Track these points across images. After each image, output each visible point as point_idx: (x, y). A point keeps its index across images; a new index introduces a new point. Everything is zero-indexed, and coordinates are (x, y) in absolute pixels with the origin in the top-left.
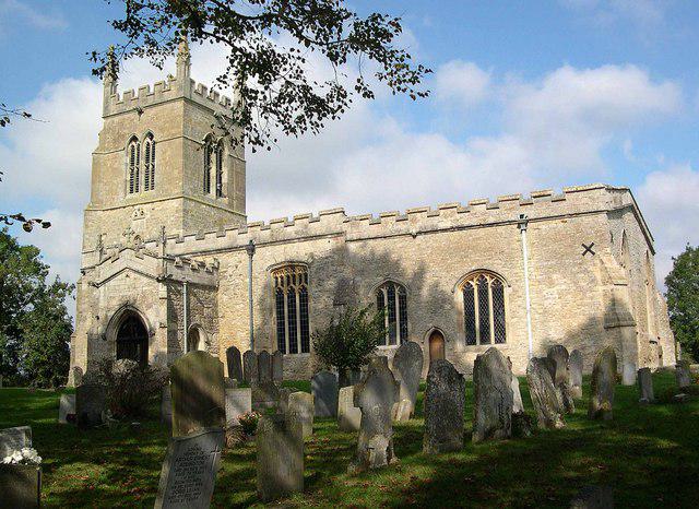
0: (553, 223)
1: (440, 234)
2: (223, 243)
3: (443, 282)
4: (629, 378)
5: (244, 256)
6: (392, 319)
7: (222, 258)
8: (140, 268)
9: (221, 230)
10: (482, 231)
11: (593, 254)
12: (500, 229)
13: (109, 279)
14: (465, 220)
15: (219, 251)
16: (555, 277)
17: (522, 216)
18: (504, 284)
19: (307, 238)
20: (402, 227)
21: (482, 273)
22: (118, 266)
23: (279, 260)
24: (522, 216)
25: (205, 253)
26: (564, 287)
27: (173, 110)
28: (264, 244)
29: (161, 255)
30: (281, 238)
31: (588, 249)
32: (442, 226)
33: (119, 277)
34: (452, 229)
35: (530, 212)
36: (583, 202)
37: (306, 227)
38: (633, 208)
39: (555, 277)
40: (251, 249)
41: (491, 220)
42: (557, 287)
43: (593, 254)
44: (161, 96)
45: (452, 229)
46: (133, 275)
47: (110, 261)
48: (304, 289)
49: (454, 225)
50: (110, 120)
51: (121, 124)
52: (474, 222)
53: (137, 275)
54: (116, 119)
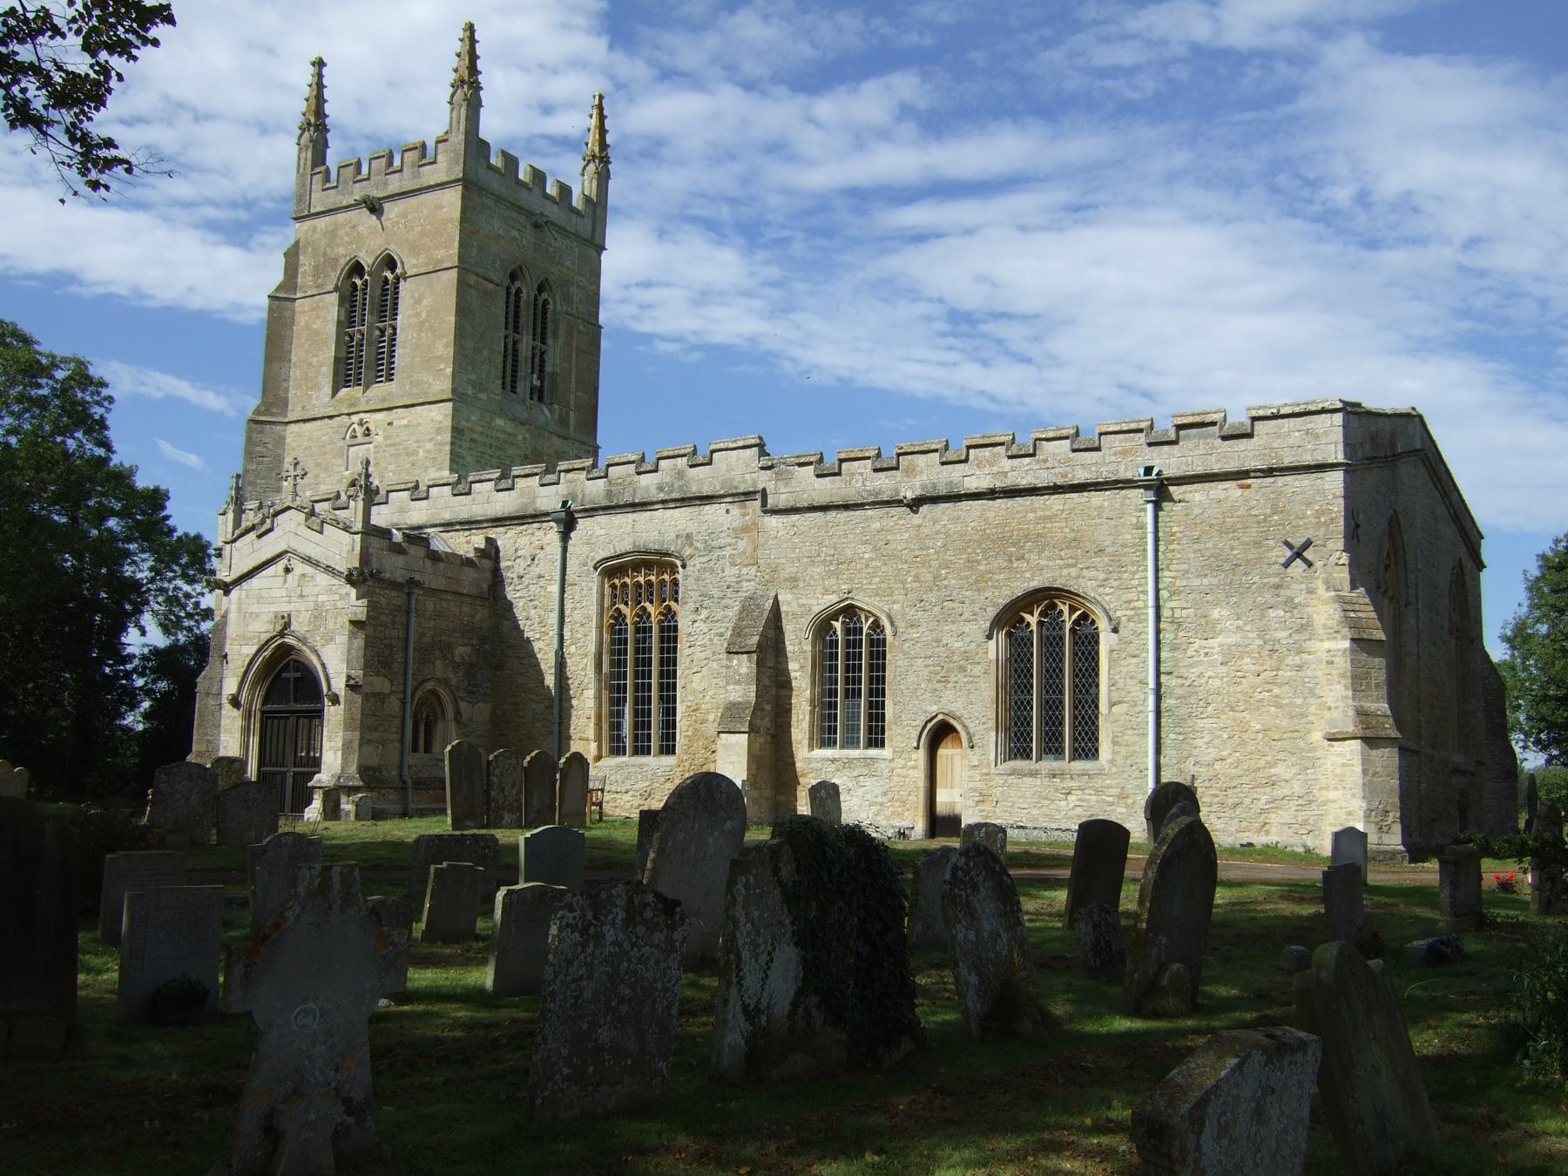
0: (1219, 489)
1: (965, 505)
2: (505, 503)
3: (1301, 570)
4: (1402, 848)
5: (550, 535)
6: (851, 694)
7: (506, 539)
8: (315, 553)
9: (503, 477)
10: (1056, 501)
11: (1310, 564)
12: (1096, 498)
13: (249, 575)
14: (1023, 473)
15: (498, 521)
16: (1215, 613)
17: (1148, 470)
18: (1103, 625)
19: (686, 501)
20: (885, 484)
21: (1046, 597)
22: (270, 546)
23: (621, 549)
24: (1148, 470)
25: (469, 524)
26: (1232, 640)
27: (440, 207)
28: (591, 512)
29: (358, 526)
30: (627, 498)
31: (1299, 555)
32: (972, 484)
33: (271, 570)
34: (991, 494)
35: (1168, 462)
36: (1288, 442)
37: (680, 474)
38: (388, 492)
39: (1215, 613)
40: (568, 523)
41: (1081, 476)
42: (1220, 639)
43: (1310, 564)
44: (417, 176)
45: (991, 494)
46: (299, 568)
47: (252, 535)
48: (669, 614)
49: (999, 484)
50: (307, 224)
51: (332, 233)
52: (1043, 478)
53: (308, 569)
54: (322, 223)
